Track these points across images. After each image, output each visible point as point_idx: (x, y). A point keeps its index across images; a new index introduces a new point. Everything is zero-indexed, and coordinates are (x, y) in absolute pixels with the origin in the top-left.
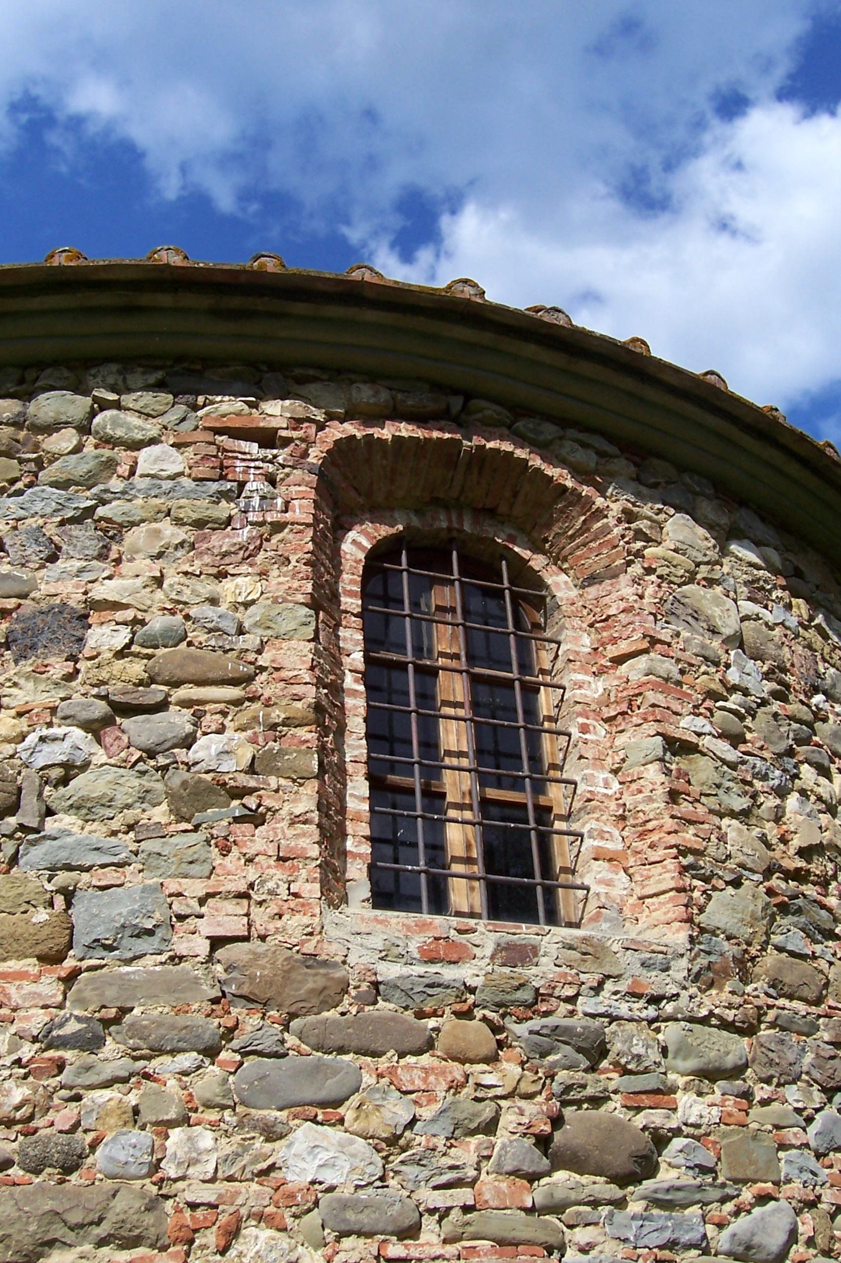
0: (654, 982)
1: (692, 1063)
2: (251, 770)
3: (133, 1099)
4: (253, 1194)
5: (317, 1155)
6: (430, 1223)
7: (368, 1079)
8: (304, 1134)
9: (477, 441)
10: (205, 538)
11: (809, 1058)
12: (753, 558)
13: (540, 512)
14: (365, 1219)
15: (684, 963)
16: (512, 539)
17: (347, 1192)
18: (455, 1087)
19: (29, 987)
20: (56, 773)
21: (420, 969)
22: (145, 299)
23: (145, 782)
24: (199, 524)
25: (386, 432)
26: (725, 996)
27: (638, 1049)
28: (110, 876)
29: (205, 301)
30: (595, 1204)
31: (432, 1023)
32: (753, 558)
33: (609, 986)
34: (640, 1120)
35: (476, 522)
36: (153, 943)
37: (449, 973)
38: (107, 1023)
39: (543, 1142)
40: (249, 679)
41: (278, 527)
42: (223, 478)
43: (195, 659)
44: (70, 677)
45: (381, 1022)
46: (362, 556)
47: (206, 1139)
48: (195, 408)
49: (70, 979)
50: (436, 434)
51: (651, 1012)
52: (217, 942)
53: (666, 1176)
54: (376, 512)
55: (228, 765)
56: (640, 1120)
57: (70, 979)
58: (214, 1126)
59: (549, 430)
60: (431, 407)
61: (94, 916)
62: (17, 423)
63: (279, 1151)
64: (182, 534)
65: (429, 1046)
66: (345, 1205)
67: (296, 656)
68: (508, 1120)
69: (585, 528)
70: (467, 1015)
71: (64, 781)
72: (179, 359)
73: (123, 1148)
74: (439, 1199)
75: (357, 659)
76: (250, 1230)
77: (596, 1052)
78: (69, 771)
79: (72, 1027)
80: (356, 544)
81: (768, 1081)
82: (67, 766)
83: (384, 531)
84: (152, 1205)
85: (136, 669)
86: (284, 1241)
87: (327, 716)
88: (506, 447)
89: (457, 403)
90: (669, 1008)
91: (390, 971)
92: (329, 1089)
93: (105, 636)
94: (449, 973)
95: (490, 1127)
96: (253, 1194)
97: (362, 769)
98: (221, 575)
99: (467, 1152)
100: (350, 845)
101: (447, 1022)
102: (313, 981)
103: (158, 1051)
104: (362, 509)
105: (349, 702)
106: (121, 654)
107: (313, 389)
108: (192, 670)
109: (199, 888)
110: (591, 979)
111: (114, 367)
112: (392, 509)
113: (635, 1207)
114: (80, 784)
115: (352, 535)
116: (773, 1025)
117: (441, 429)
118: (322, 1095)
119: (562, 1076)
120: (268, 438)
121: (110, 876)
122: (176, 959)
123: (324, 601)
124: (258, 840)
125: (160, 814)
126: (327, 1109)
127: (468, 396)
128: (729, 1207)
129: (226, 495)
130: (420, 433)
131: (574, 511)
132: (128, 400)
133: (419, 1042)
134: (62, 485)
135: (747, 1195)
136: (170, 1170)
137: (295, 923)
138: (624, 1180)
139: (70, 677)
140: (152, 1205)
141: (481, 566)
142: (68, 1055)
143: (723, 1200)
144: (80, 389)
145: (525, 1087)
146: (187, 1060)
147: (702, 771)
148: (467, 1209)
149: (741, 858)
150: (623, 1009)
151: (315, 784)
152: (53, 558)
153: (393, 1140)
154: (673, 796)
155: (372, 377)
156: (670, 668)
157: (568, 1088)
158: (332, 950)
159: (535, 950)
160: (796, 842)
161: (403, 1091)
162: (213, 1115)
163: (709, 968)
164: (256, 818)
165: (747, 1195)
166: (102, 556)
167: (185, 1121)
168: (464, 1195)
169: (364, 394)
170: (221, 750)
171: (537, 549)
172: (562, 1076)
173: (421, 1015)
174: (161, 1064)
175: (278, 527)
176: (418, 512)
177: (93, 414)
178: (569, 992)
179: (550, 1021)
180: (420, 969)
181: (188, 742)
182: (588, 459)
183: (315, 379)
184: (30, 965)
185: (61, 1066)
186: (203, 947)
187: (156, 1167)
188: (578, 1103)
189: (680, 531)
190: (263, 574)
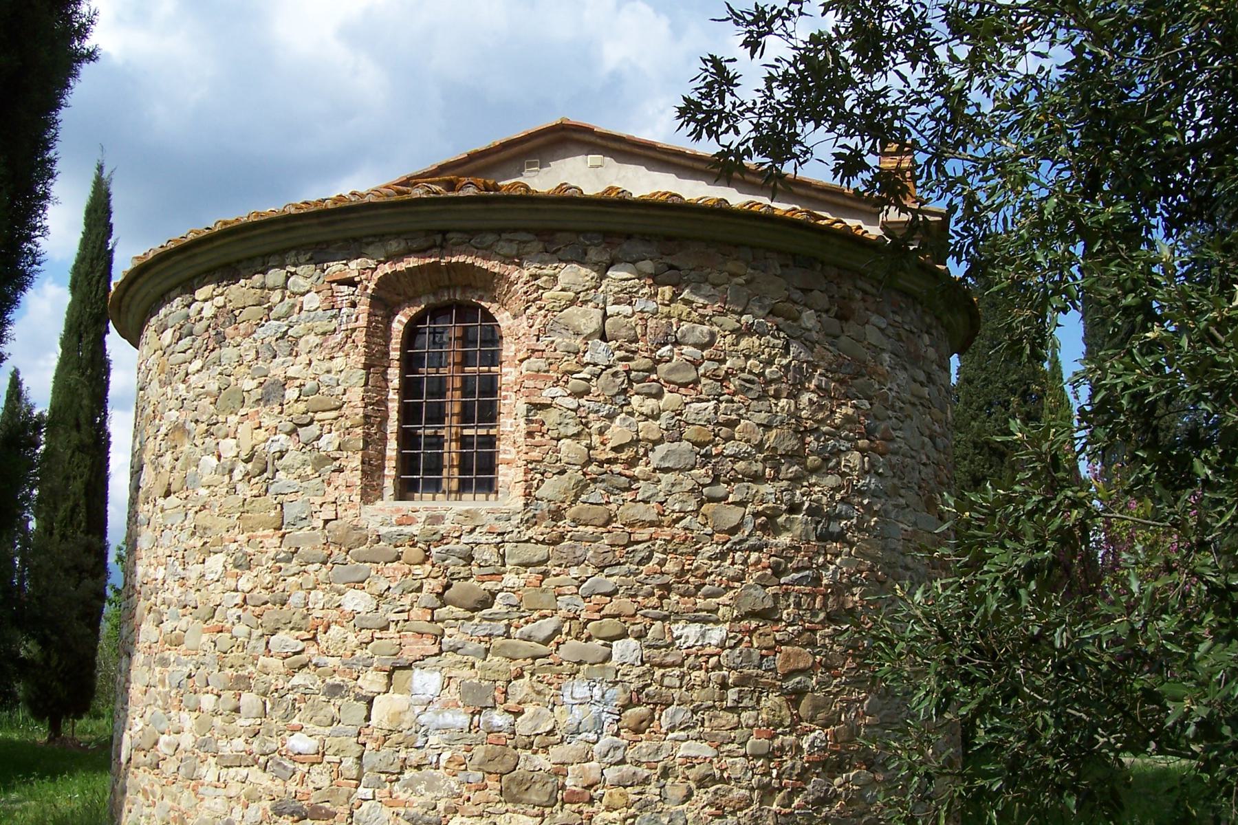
0: (501, 526)
1: (515, 561)
2: (339, 449)
3: (300, 581)
4: (334, 614)
5: (357, 601)
6: (392, 625)
7: (373, 573)
8: (351, 593)
9: (447, 259)
10: (326, 340)
11: (590, 553)
12: (626, 275)
13: (489, 284)
14: (368, 624)
15: (520, 516)
16: (481, 298)
17: (363, 614)
18: (405, 575)
19: (270, 540)
20: (277, 455)
21: (395, 529)
22: (292, 224)
23: (305, 457)
24: (324, 334)
25: (401, 266)
26: (542, 529)
27: (487, 557)
28: (293, 497)
29: (315, 221)
30: (457, 620)
31: (400, 549)
32: (626, 275)
33: (478, 530)
34: (483, 586)
35: (463, 292)
36: (304, 523)
37: (406, 530)
38: (293, 553)
39: (440, 595)
40: (340, 407)
41: (354, 330)
42: (333, 308)
43: (321, 401)
44: (281, 413)
45: (378, 551)
46: (401, 328)
47: (321, 594)
48: (324, 271)
49: (283, 536)
50: (427, 261)
51: (499, 539)
52: (326, 522)
53: (495, 608)
54: (411, 300)
55: (330, 448)
56: (483, 586)
57: (283, 536)
58: (323, 590)
59: (490, 238)
60: (426, 245)
61: (291, 512)
62: (263, 287)
63: (343, 600)
64: (318, 340)
65: (398, 558)
66: (362, 619)
67: (356, 395)
68: (425, 587)
69: (509, 291)
70: (414, 545)
71: (281, 457)
72: (318, 243)
73: (297, 598)
74: (395, 617)
75: (395, 382)
76: (333, 626)
77: (468, 559)
78: (282, 454)
79: (282, 555)
80: (399, 323)
81: (560, 566)
82: (281, 451)
83: (415, 310)
84: (305, 617)
85: (301, 407)
86: (343, 630)
87: (374, 418)
88: (462, 259)
89: (439, 239)
90: (507, 537)
91: (383, 530)
92: (359, 577)
93: (291, 393)
94: (406, 530)
95: (419, 589)
96: (334, 614)
97: (394, 436)
98: (332, 358)
99: (407, 601)
100: (386, 472)
101: (406, 549)
102: (355, 536)
103: (307, 563)
104: (404, 302)
105: (390, 405)
106: (297, 401)
107: (370, 250)
108: (320, 406)
109: (319, 500)
110: (467, 528)
111: (293, 253)
112: (420, 297)
113: (476, 621)
114: (287, 460)
115: (398, 317)
116: (570, 539)
117: (430, 257)
118: (357, 579)
119: (451, 569)
120: (351, 282)
121: (293, 497)
122: (314, 529)
123: (375, 363)
124: (339, 479)
125: (309, 470)
126: (359, 584)
127: (444, 232)
128: (523, 620)
129: (335, 317)
130: (421, 262)
131: (502, 282)
132: (299, 270)
133: (392, 558)
134: (278, 319)
135: (536, 615)
136: (311, 606)
137: (351, 512)
138: (474, 610)
139: (281, 413)
140: (305, 617)
141: (467, 312)
142: (282, 565)
143: (521, 618)
144: (282, 267)
145: (433, 574)
146: (317, 566)
147: (551, 417)
148: (405, 621)
149: (566, 460)
150: (483, 540)
151: (360, 453)
152: (275, 357)
153: (381, 595)
154: (530, 434)
155: (398, 235)
156: (542, 364)
157: (452, 574)
158: (363, 523)
159: (443, 517)
160: (609, 446)
161: (388, 576)
162: (324, 586)
163: (534, 516)
164: (340, 470)
165: (536, 615)
166: (290, 354)
167: (315, 588)
168: (405, 616)
169: (394, 246)
170: (329, 442)
171: (493, 300)
172: (451, 569)
173: (396, 546)
174: (310, 568)
175: (354, 330)
176: (435, 294)
177: (287, 278)
178: (457, 534)
179: (447, 547)
180: (395, 529)
181: (318, 438)
182: (506, 249)
183: (372, 243)
184: (270, 532)
185: (280, 569)
186: (321, 524)
187: (307, 604)
188: (459, 579)
189: (573, 275)
190: (347, 355)
